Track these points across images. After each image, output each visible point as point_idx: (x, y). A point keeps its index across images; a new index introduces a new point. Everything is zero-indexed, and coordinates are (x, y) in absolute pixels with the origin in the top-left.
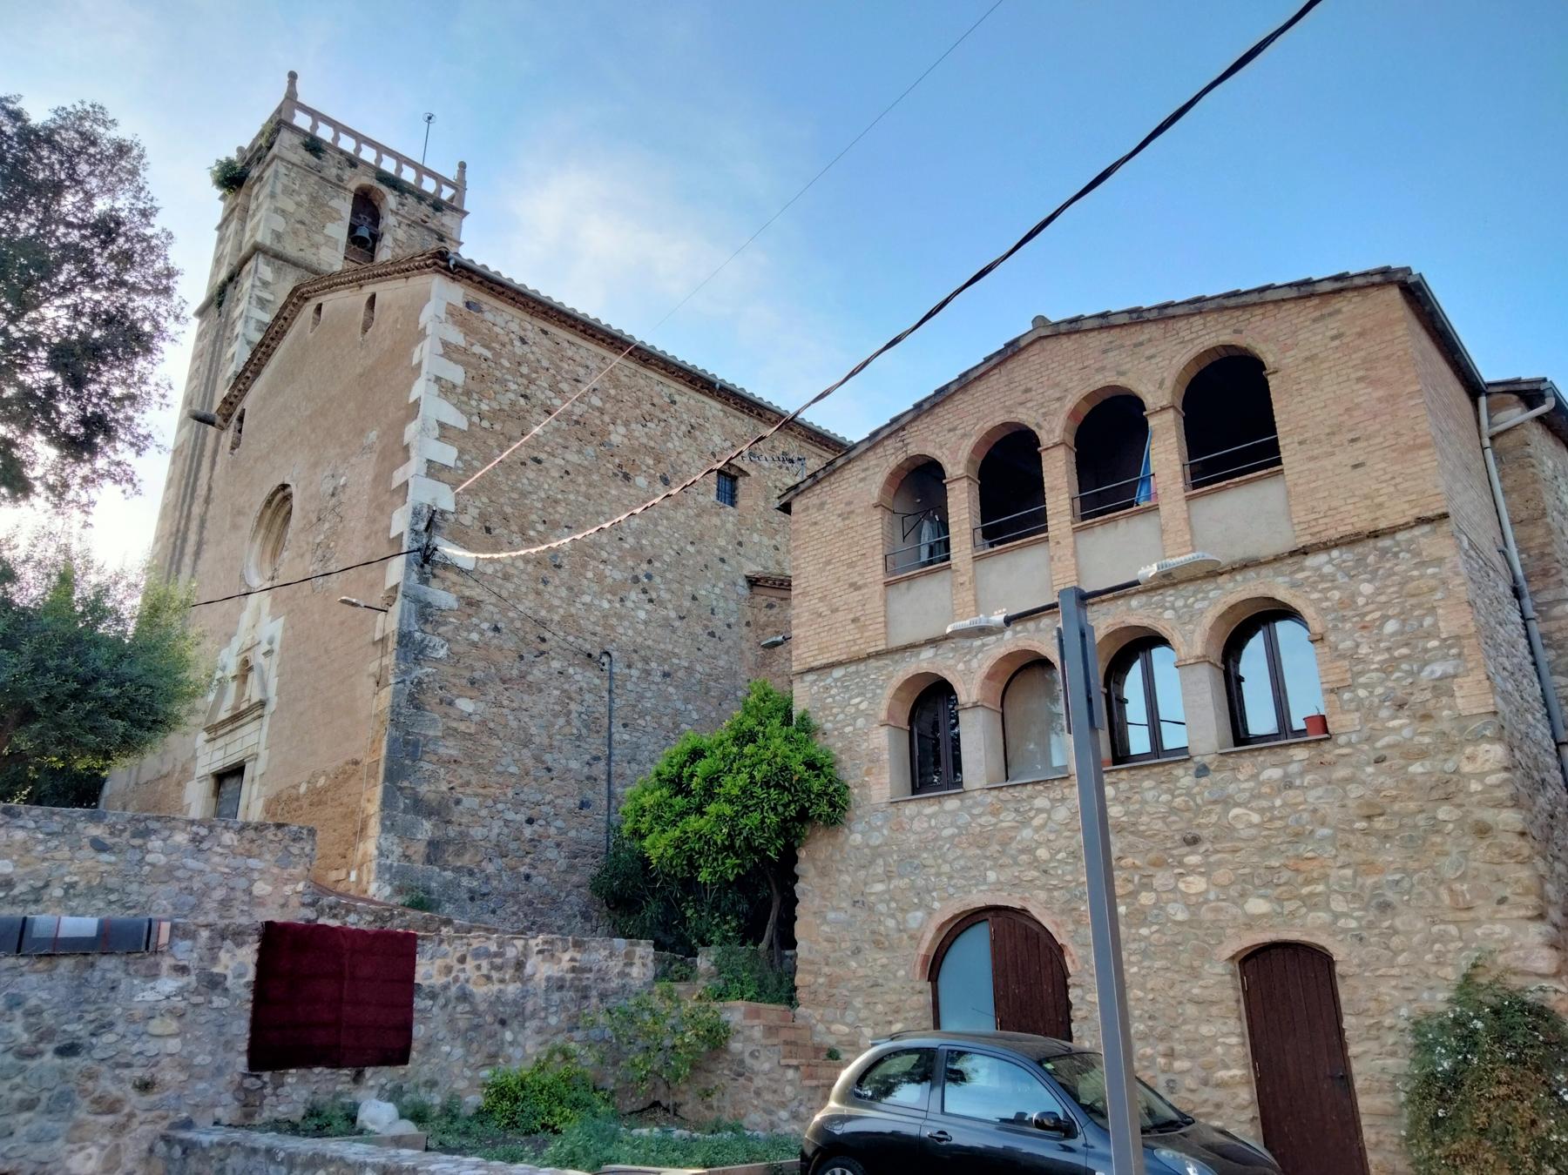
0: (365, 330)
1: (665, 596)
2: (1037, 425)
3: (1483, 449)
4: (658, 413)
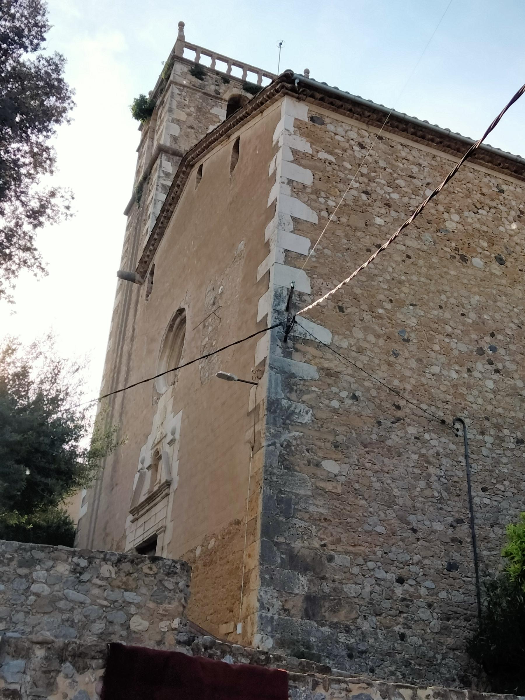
1: (512, 367)
4: (488, 201)
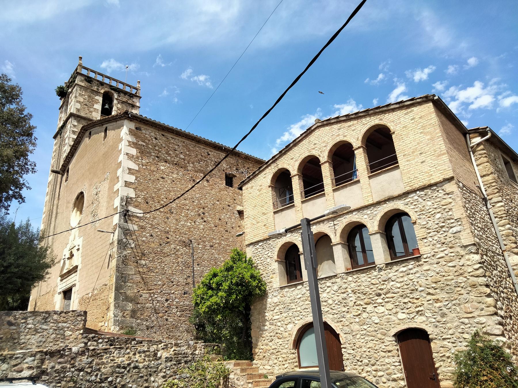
2: (319, 155)
3: (469, 152)
4: (204, 159)
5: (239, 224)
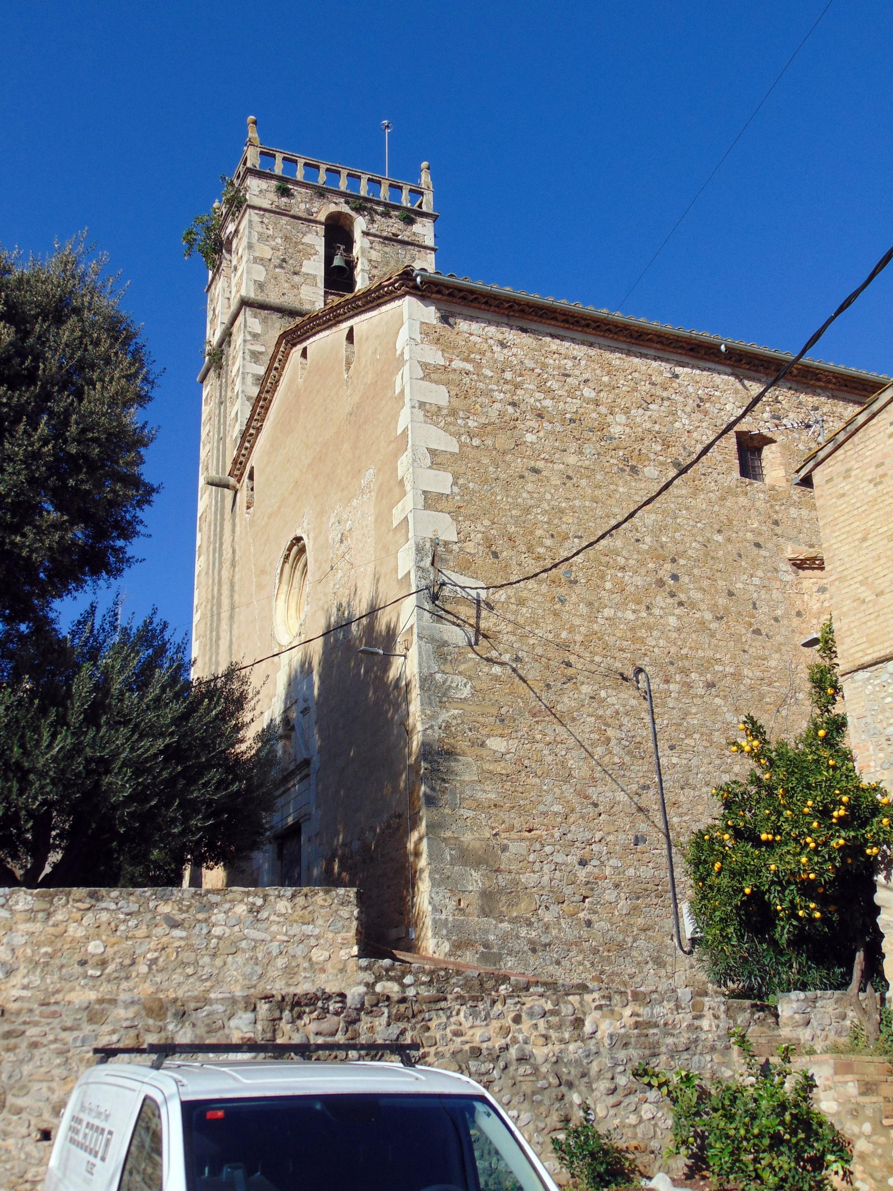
0: (348, 370)
1: (697, 596)
4: (659, 391)
5: (799, 605)
